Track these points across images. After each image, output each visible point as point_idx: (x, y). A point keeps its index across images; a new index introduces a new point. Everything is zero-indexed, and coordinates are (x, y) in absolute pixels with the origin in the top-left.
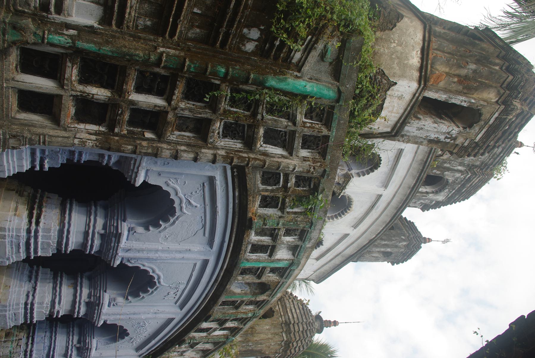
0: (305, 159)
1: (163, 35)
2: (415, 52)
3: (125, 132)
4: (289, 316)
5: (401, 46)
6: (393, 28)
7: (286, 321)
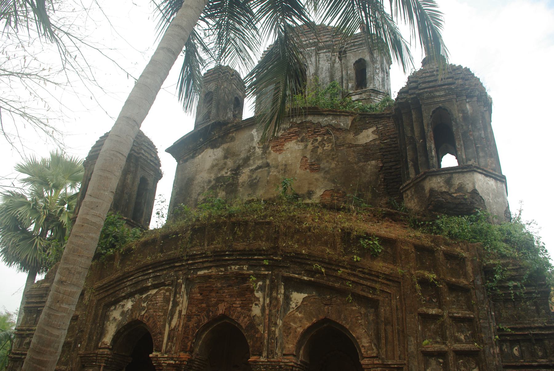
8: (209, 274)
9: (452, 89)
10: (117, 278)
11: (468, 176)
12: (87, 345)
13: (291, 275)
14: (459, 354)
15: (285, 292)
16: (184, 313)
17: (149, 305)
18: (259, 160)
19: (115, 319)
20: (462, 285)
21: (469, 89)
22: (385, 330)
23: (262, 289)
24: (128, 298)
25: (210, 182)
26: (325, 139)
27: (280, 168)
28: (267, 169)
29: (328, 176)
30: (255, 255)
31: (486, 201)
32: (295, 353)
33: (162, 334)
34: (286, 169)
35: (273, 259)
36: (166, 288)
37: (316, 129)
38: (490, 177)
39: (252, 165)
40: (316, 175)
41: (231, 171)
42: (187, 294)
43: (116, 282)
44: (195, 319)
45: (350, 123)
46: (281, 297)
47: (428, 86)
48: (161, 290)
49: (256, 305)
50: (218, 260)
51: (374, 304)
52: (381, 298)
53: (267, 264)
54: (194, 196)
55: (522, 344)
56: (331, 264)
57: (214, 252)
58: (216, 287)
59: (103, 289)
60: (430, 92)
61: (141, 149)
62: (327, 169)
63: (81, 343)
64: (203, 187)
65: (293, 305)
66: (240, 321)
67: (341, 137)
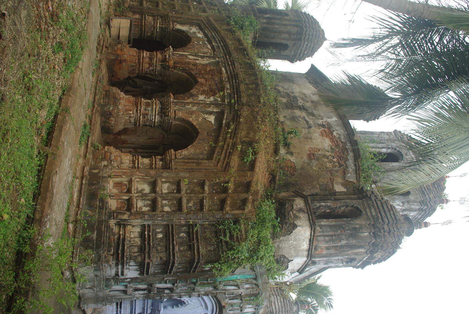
0: (247, 289)
1: (166, 273)
2: (305, 243)
3: (156, 292)
4: (272, 308)
5: (296, 241)
6: (291, 233)
7: (270, 311)
8: (223, 73)
9: (378, 220)
10: (216, 27)
11: (307, 223)
12: (174, 17)
13: (226, 114)
14: (180, 202)
15: (214, 112)
16: (197, 62)
17: (201, 45)
18: (313, 122)
19: (191, 29)
20: (225, 206)
21: (380, 233)
22: (193, 162)
23: (216, 100)
24: (204, 35)
25: (293, 93)
26: (335, 164)
27: (309, 135)
28: (307, 127)
29: (306, 165)
30: (237, 94)
31: (290, 237)
32: (176, 117)
33: (184, 51)
34: (308, 138)
35: (235, 105)
36: (212, 53)
37: (342, 157)
38: (310, 245)
39: (308, 118)
40: (305, 158)
41: (302, 105)
42: (209, 63)
43: (213, 27)
44: (193, 67)
45: (351, 180)
46: (210, 109)
47: (379, 205)
48: (211, 50)
49: (205, 97)
50: (232, 77)
51: (210, 157)
52: (213, 161)
53: (232, 102)
54: (281, 84)
55: (187, 238)
56: (235, 134)
57: (237, 74)
58: (215, 78)
59: (209, 22)
60: (373, 206)
61: (308, 41)
62: (311, 164)
63: (175, 13)
64: (288, 89)
65: (206, 116)
66: (194, 90)
67: (338, 174)
